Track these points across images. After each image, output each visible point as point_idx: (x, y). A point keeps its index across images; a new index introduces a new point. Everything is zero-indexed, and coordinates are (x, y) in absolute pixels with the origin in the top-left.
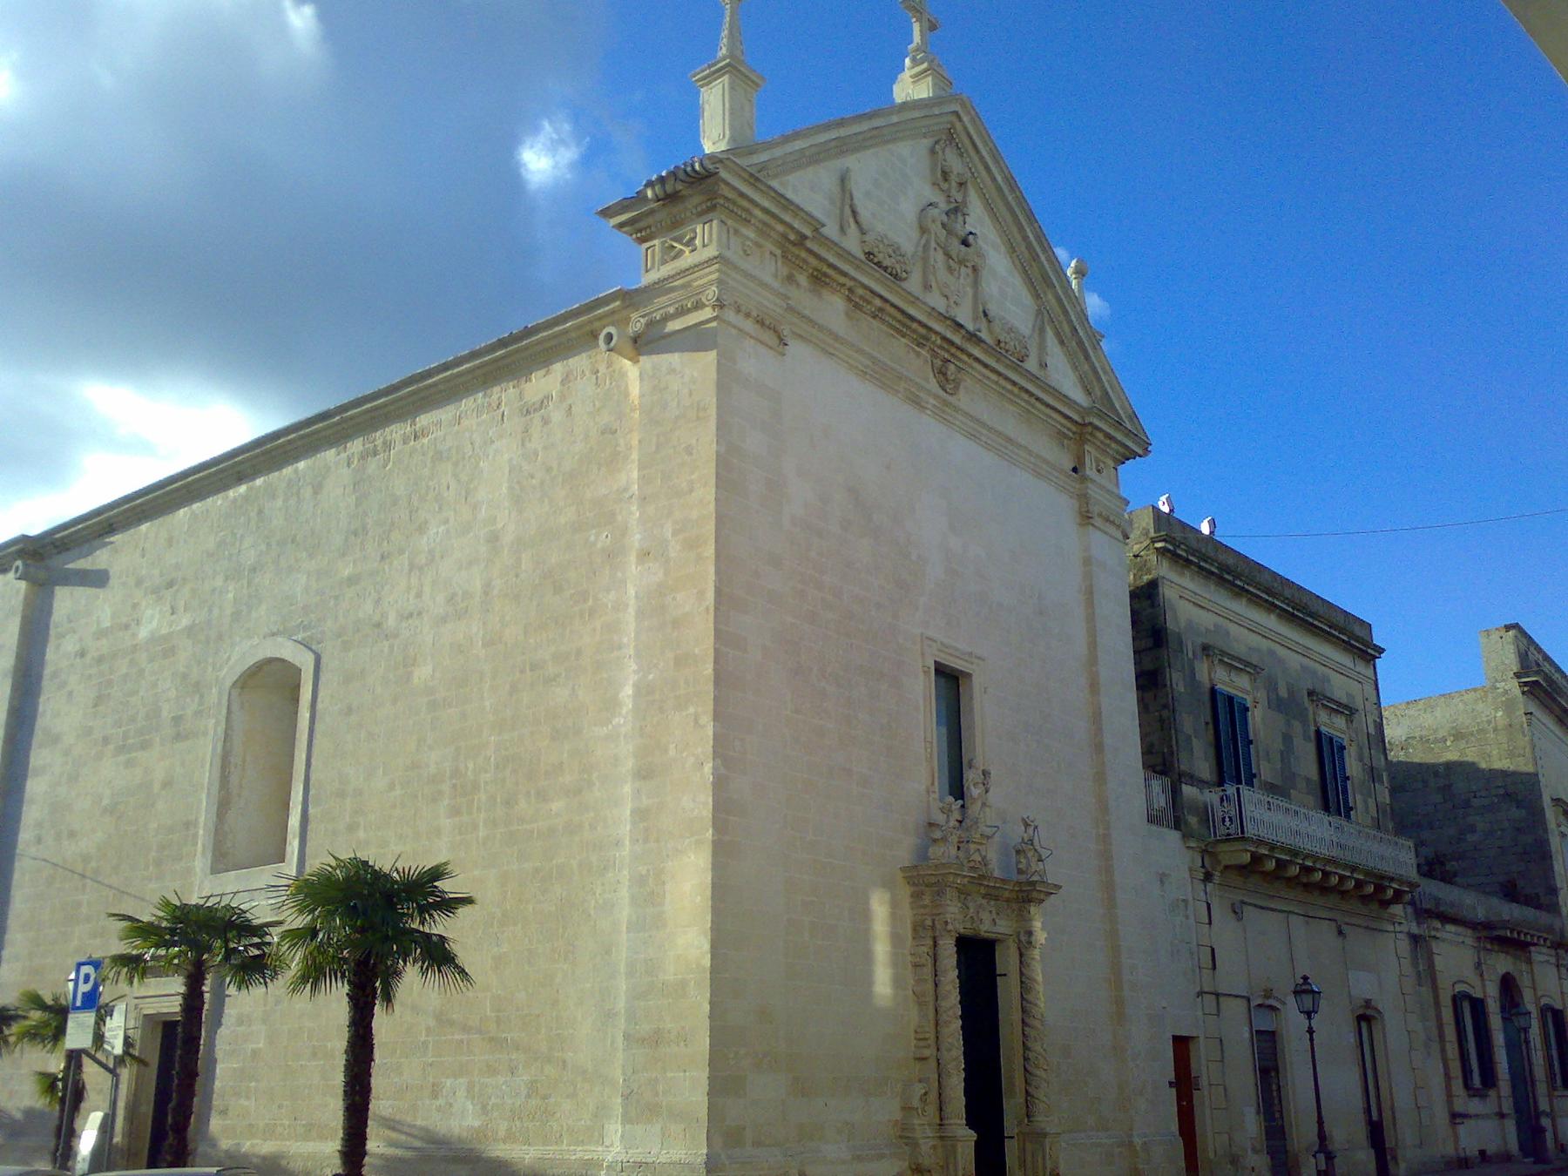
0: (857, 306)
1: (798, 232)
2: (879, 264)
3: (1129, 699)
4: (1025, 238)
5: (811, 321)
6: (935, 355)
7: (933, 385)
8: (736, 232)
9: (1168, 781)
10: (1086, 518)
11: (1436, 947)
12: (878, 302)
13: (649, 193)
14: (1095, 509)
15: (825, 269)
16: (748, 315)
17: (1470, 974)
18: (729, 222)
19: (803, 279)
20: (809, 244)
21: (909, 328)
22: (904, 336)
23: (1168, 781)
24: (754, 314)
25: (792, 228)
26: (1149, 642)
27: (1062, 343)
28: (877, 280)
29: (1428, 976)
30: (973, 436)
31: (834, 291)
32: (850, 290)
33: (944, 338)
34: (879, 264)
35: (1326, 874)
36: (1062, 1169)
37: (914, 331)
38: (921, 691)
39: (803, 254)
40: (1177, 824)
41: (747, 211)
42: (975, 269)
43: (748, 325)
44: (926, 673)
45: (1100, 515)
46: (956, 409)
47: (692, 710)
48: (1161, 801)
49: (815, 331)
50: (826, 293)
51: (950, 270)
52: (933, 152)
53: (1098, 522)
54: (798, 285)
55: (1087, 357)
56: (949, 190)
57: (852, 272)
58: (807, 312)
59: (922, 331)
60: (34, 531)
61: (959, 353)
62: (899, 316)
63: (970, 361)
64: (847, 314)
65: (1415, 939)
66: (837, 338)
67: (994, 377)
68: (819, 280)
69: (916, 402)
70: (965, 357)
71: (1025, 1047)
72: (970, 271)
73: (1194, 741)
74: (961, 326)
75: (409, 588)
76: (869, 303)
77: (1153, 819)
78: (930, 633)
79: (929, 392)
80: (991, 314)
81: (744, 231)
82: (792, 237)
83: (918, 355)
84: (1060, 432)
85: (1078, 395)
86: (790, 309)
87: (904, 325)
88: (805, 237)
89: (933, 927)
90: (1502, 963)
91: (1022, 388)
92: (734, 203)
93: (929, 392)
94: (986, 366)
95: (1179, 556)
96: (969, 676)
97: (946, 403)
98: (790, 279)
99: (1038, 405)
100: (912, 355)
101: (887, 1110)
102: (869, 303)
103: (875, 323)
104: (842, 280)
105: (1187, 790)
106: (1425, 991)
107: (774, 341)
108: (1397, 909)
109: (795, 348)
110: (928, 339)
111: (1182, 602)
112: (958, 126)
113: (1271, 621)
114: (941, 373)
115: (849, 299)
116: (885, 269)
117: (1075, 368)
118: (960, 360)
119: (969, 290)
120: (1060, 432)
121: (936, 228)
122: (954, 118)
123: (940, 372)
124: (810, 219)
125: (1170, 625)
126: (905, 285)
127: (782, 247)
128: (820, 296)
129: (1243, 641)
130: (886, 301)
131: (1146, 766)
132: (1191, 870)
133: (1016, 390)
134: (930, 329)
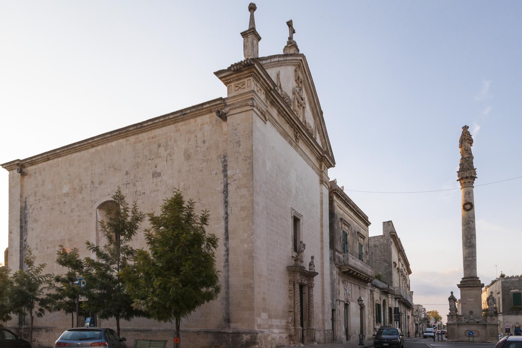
11: (374, 293)
13: (232, 69)
17: (378, 299)
29: (372, 299)
31: (275, 107)
35: (360, 275)
36: (404, 346)
38: (291, 222)
41: (259, 78)
43: (259, 113)
47: (247, 221)
51: (298, 106)
52: (296, 71)
53: (324, 183)
60: (21, 158)
65: (371, 291)
71: (309, 310)
75: (153, 183)
89: (294, 282)
90: (384, 297)
101: (284, 322)
105: (337, 253)
106: (372, 302)
107: (264, 119)
108: (369, 284)
113: (352, 214)
122: (300, 62)
129: (347, 218)
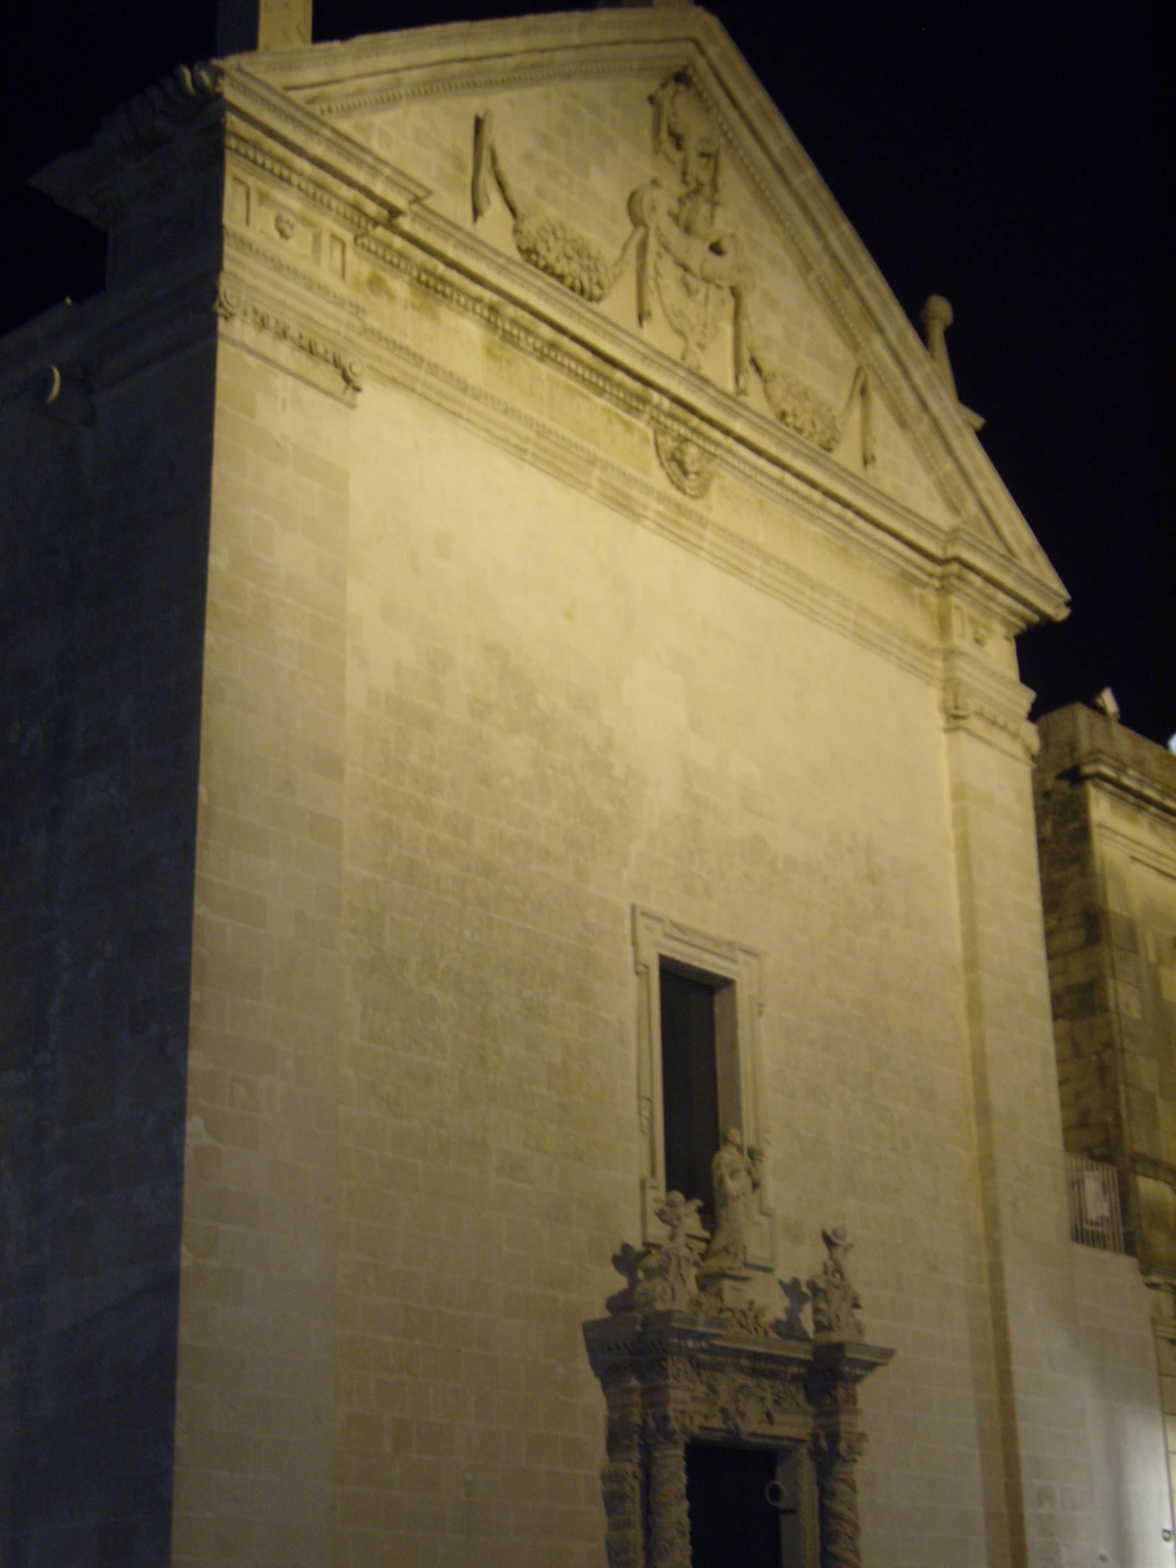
0: (507, 337)
1: (382, 203)
2: (548, 269)
3: (1040, 1031)
4: (827, 248)
5: (414, 355)
6: (661, 431)
7: (658, 478)
8: (264, 198)
9: (1110, 1172)
10: (954, 718)
12: (546, 331)
14: (972, 704)
15: (441, 269)
16: (283, 334)
18: (251, 181)
19: (400, 287)
20: (405, 223)
21: (608, 379)
22: (600, 392)
23: (1110, 1172)
24: (294, 332)
25: (370, 195)
26: (1073, 937)
27: (903, 424)
28: (541, 293)
30: (736, 570)
32: (493, 309)
33: (677, 401)
34: (548, 269)
37: (620, 386)
39: (398, 242)
40: (1130, 1246)
41: (281, 161)
42: (735, 292)
44: (641, 972)
45: (980, 714)
46: (702, 521)
48: (1098, 1204)
49: (422, 374)
50: (448, 316)
53: (975, 723)
54: (391, 296)
55: (950, 450)
56: (685, 162)
57: (492, 276)
58: (408, 342)
59: (636, 386)
61: (705, 428)
62: (587, 356)
63: (729, 442)
64: (490, 353)
66: (464, 388)
67: (775, 472)
68: (431, 288)
69: (623, 505)
70: (717, 435)
72: (726, 294)
73: (1160, 1103)
74: (706, 381)
76: (528, 332)
77: (1082, 1235)
78: (652, 905)
79: (648, 490)
80: (766, 368)
81: (278, 195)
82: (372, 208)
83: (629, 427)
84: (904, 573)
85: (942, 518)
86: (366, 331)
87: (600, 375)
88: (394, 212)
91: (828, 494)
92: (257, 147)
93: (648, 490)
94: (758, 451)
95: (1125, 789)
96: (727, 984)
97: (680, 510)
98: (375, 284)
99: (860, 523)
100: (618, 428)
102: (528, 332)
103: (544, 369)
104: (477, 290)
109: (372, 395)
110: (645, 401)
111: (1137, 868)
112: (701, 63)
114: (676, 463)
115: (491, 325)
116: (561, 278)
117: (930, 469)
118: (707, 438)
119: (728, 330)
120: (904, 573)
121: (660, 220)
122: (691, 48)
123: (673, 458)
124: (399, 178)
125: (1114, 904)
126: (603, 307)
127: (353, 225)
128: (434, 317)
130: (562, 330)
131: (1068, 1147)
132: (1154, 1322)
133: (817, 496)
134: (647, 383)
